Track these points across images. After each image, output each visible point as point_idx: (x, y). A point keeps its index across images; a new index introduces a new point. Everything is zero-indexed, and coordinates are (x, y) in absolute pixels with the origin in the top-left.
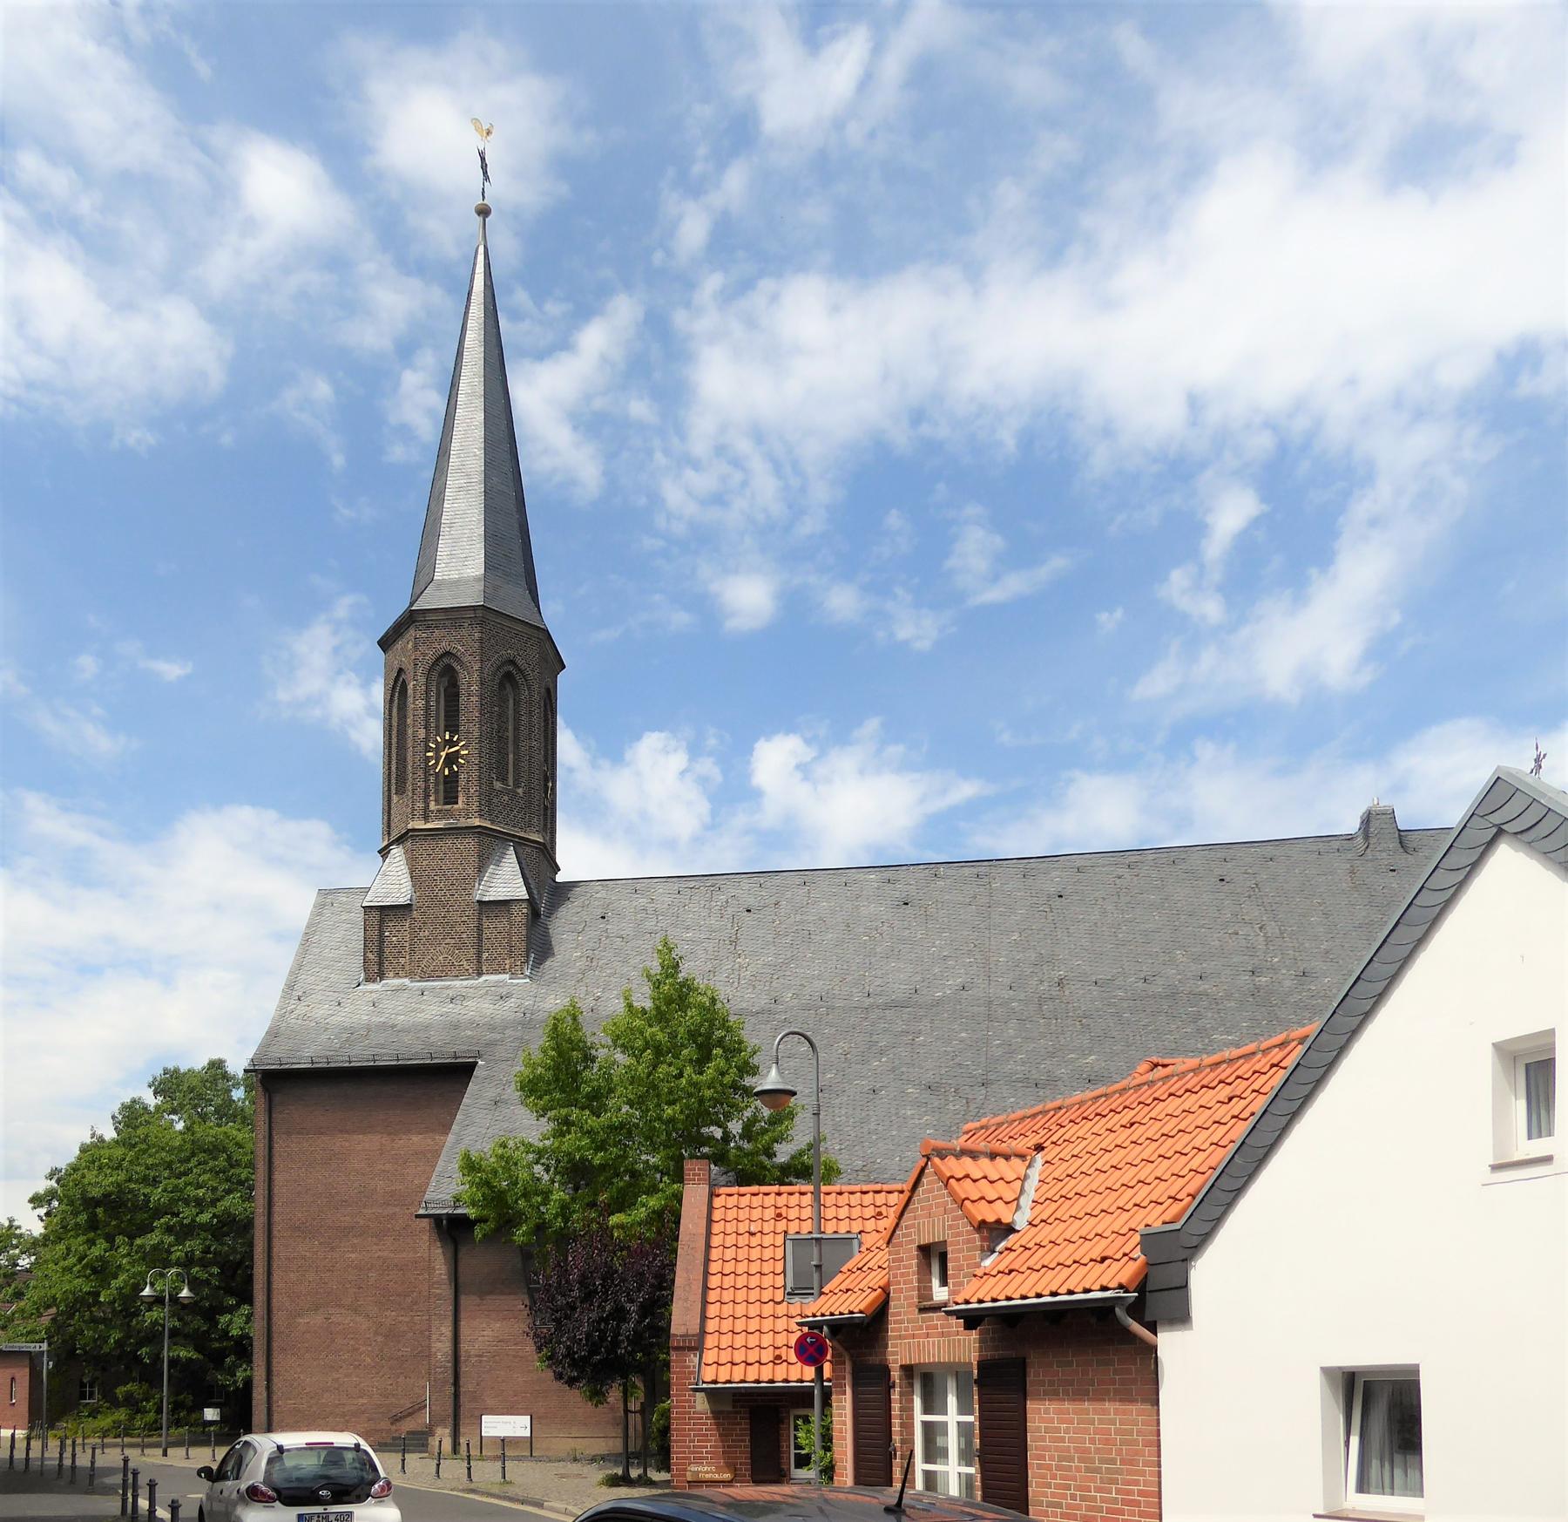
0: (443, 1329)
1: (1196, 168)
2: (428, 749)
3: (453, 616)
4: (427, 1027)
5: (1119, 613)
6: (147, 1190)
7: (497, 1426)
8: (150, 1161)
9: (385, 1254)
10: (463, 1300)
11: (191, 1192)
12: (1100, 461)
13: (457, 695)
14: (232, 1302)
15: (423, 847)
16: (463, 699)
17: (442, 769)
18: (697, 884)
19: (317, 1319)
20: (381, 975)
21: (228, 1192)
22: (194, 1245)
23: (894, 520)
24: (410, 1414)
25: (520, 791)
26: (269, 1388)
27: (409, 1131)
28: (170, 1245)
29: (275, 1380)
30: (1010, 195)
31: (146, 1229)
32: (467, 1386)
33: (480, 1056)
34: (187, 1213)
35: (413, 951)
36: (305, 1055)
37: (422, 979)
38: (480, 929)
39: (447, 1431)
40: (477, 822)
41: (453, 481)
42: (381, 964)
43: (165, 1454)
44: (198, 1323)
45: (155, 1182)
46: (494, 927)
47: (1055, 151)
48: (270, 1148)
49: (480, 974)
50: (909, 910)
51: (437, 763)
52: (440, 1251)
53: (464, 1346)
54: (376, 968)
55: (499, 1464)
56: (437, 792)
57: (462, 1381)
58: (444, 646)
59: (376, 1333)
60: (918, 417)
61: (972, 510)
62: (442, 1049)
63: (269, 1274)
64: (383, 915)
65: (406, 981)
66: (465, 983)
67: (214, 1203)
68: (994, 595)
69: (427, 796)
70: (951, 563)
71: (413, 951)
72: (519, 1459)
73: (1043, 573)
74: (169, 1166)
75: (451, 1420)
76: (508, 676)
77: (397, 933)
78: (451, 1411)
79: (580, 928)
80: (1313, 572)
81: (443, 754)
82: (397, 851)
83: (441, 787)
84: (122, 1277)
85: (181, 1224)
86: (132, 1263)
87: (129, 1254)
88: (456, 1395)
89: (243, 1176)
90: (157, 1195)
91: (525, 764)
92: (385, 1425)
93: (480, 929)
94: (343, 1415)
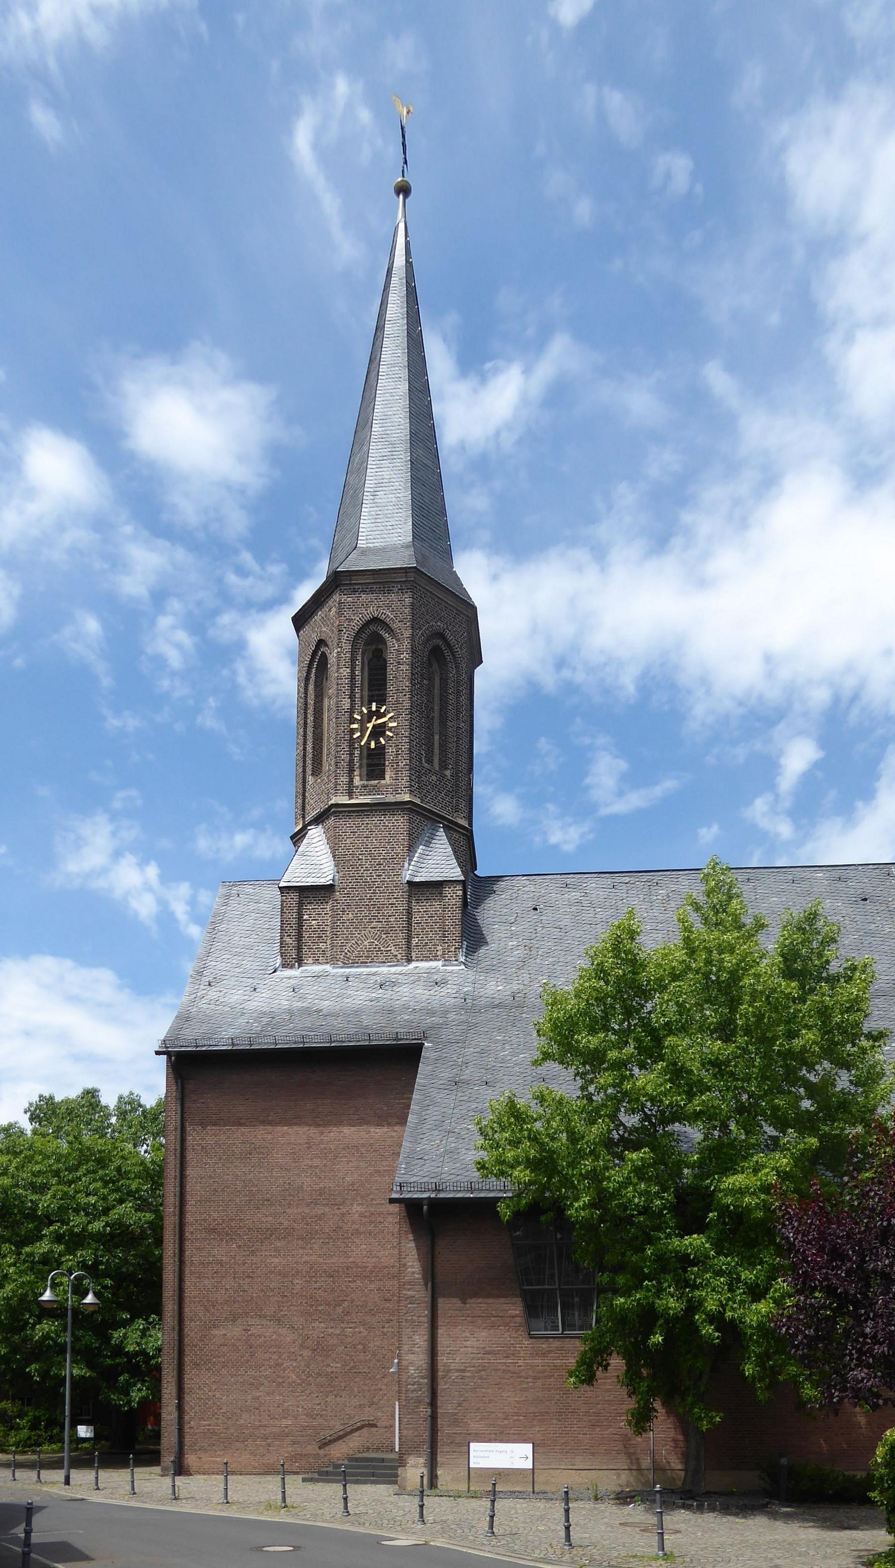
0: (417, 1339)
1: (769, 481)
2: (353, 721)
3: (381, 580)
4: (357, 1012)
5: (715, 829)
6: (34, 1197)
7: (487, 1455)
8: (37, 1168)
9: (314, 1258)
10: (441, 1301)
11: (83, 1199)
12: (700, 711)
13: (384, 667)
14: (126, 1316)
15: (347, 825)
16: (391, 669)
17: (368, 743)
18: (632, 880)
19: (235, 1331)
20: (300, 962)
21: (121, 1201)
22: (85, 1254)
23: (543, 744)
24: (340, 1438)
25: (448, 773)
26: (180, 1408)
27: (340, 1123)
28: (61, 1255)
29: (187, 1398)
30: (626, 495)
31: (35, 1237)
32: (446, 1407)
33: (426, 1038)
34: (77, 1221)
35: (335, 935)
36: (224, 1037)
37: (345, 965)
38: (409, 913)
39: (422, 1460)
40: (407, 798)
41: (376, 450)
42: (299, 949)
43: (67, 1482)
44: (89, 1339)
45: (42, 1189)
46: (423, 910)
47: (662, 463)
48: (183, 1140)
49: (409, 960)
50: (868, 906)
51: (362, 736)
52: (412, 1245)
53: (442, 1359)
54: (295, 953)
55: (417, 1500)
56: (361, 767)
57: (440, 1400)
58: (372, 611)
59: (302, 1346)
60: (561, 663)
61: (602, 740)
62: (379, 1030)
63: (181, 1280)
64: (310, 894)
65: (328, 967)
66: (393, 969)
67: (106, 1211)
68: (619, 807)
69: (351, 771)
70: (588, 781)
71: (335, 935)
72: (513, 1494)
73: (658, 791)
74: (57, 1174)
75: (426, 1447)
76: (436, 653)
77: (316, 916)
78: (426, 1435)
79: (512, 919)
80: (859, 804)
81: (370, 725)
82: (316, 834)
83: (365, 761)
84: (9, 1287)
85: (71, 1231)
86: (21, 1273)
87: (14, 1264)
88: (434, 1417)
89: (133, 1187)
90: (45, 1202)
91: (452, 747)
92: (312, 1448)
93: (409, 913)
94: (265, 1438)
